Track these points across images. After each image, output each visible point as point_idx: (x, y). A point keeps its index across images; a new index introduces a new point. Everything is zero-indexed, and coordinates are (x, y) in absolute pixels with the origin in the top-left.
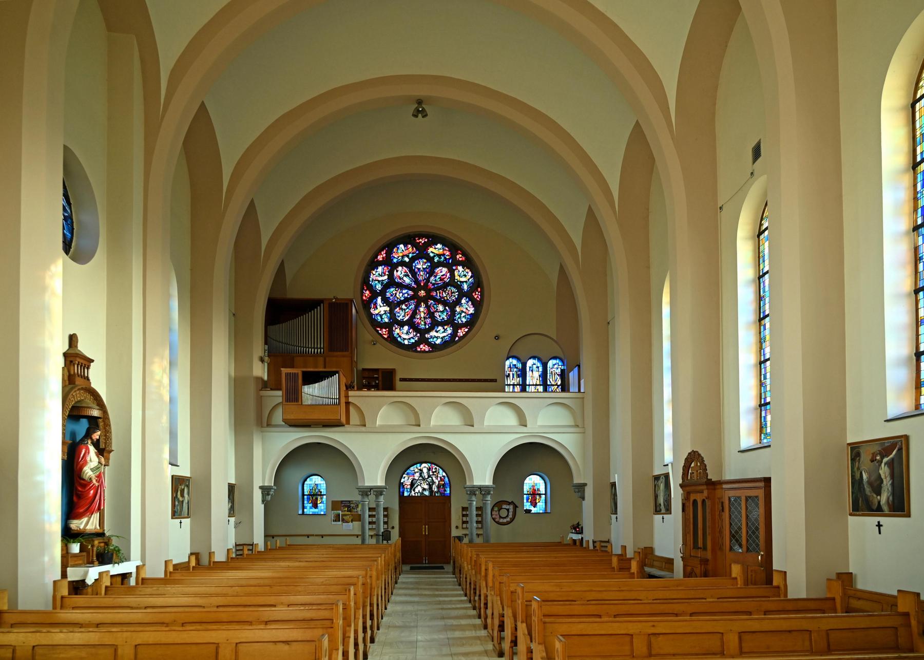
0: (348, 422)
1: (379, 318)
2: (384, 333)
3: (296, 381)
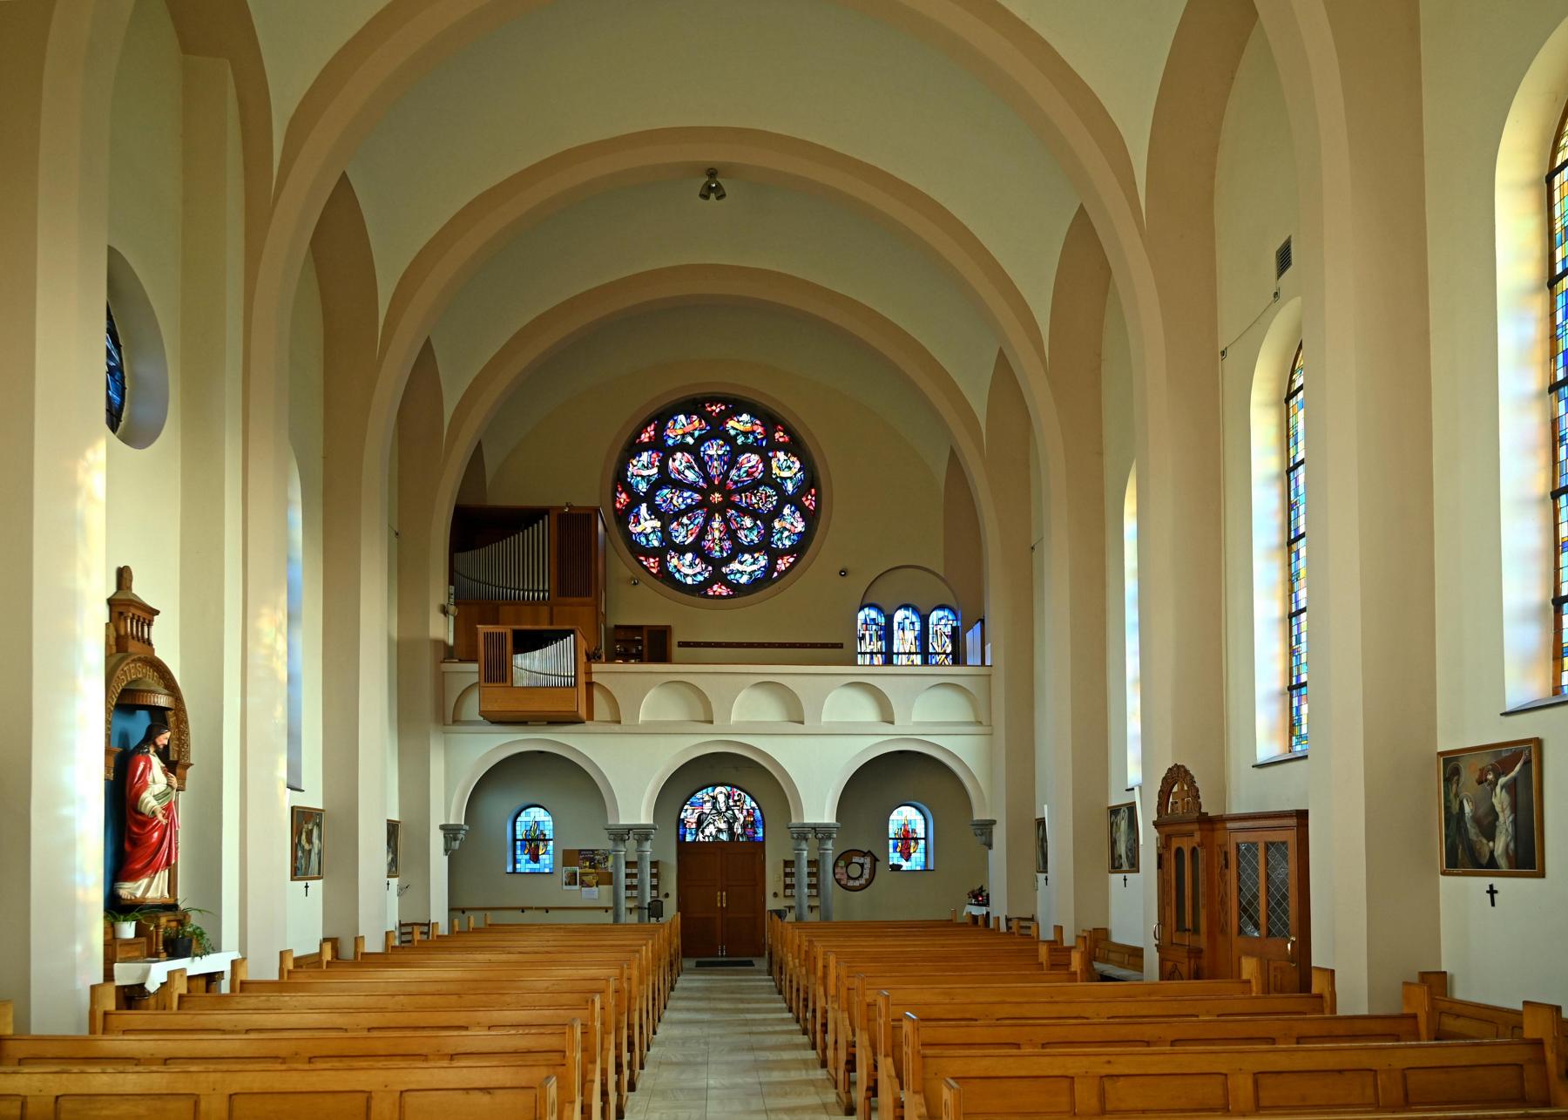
0: (590, 716)
1: (643, 539)
2: (652, 565)
3: (502, 647)
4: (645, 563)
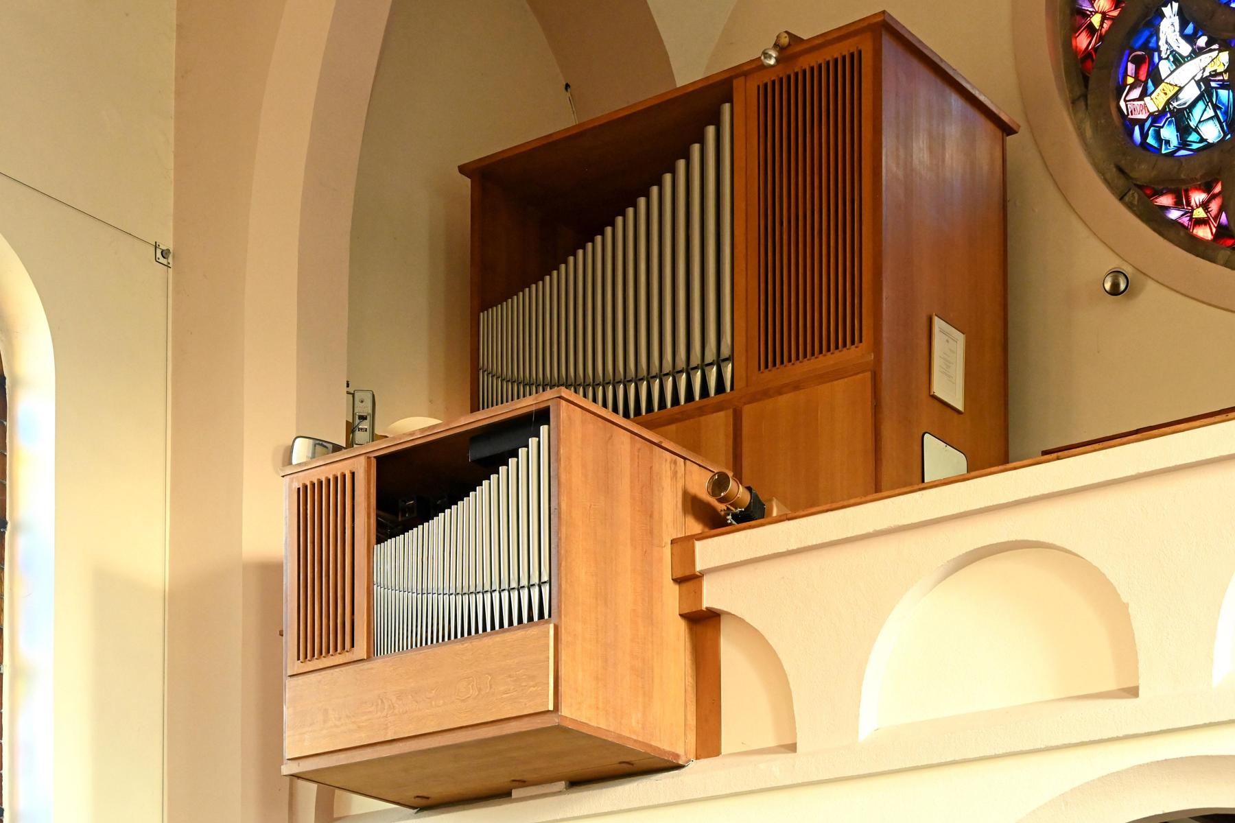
0: (709, 743)
1: (1169, 133)
2: (1199, 213)
3: (345, 516)
4: (1174, 214)
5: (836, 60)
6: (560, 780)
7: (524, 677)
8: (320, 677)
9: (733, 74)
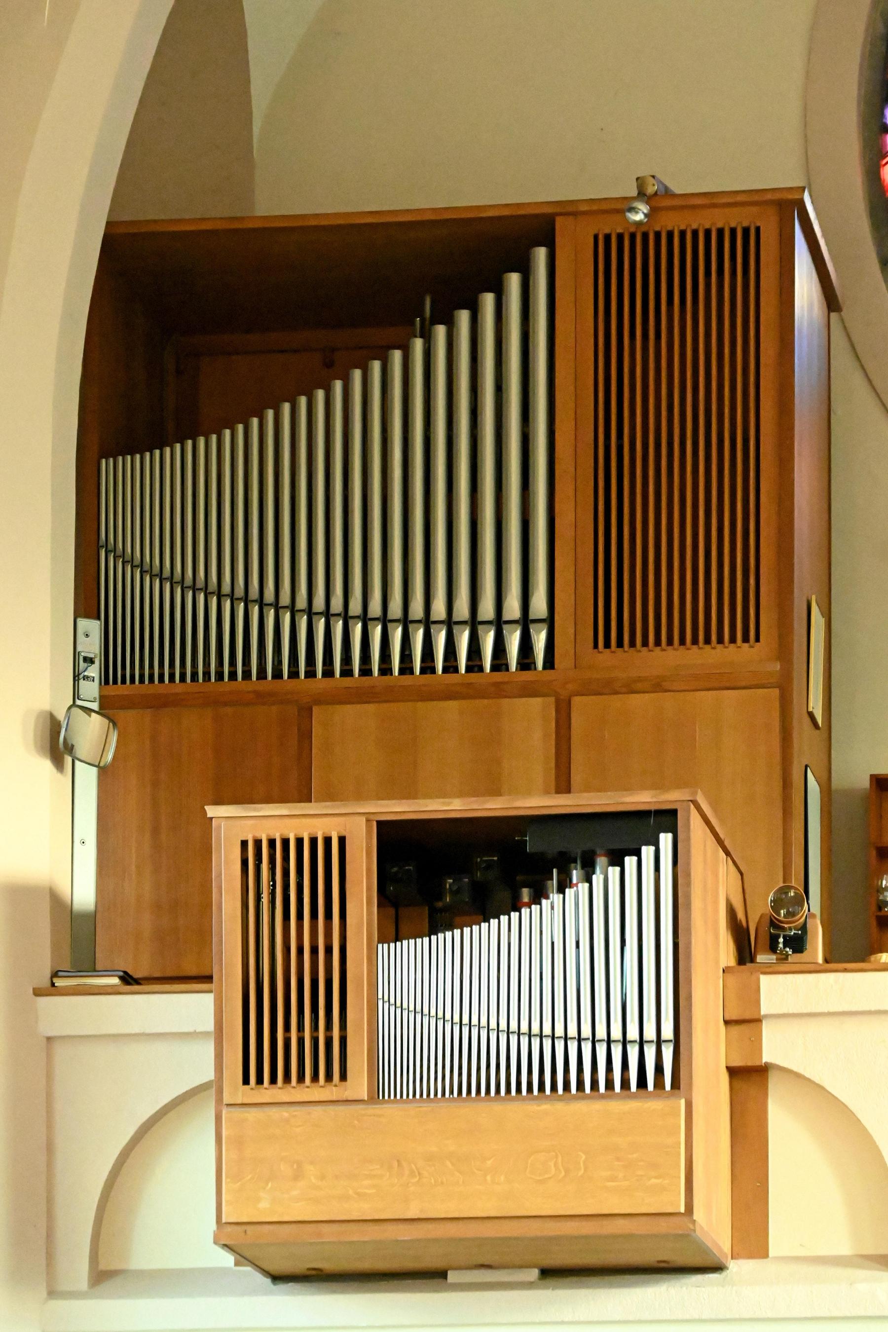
5: (720, 232)
6: (534, 1267)
7: (642, 1163)
8: (286, 1115)
9: (558, 210)
